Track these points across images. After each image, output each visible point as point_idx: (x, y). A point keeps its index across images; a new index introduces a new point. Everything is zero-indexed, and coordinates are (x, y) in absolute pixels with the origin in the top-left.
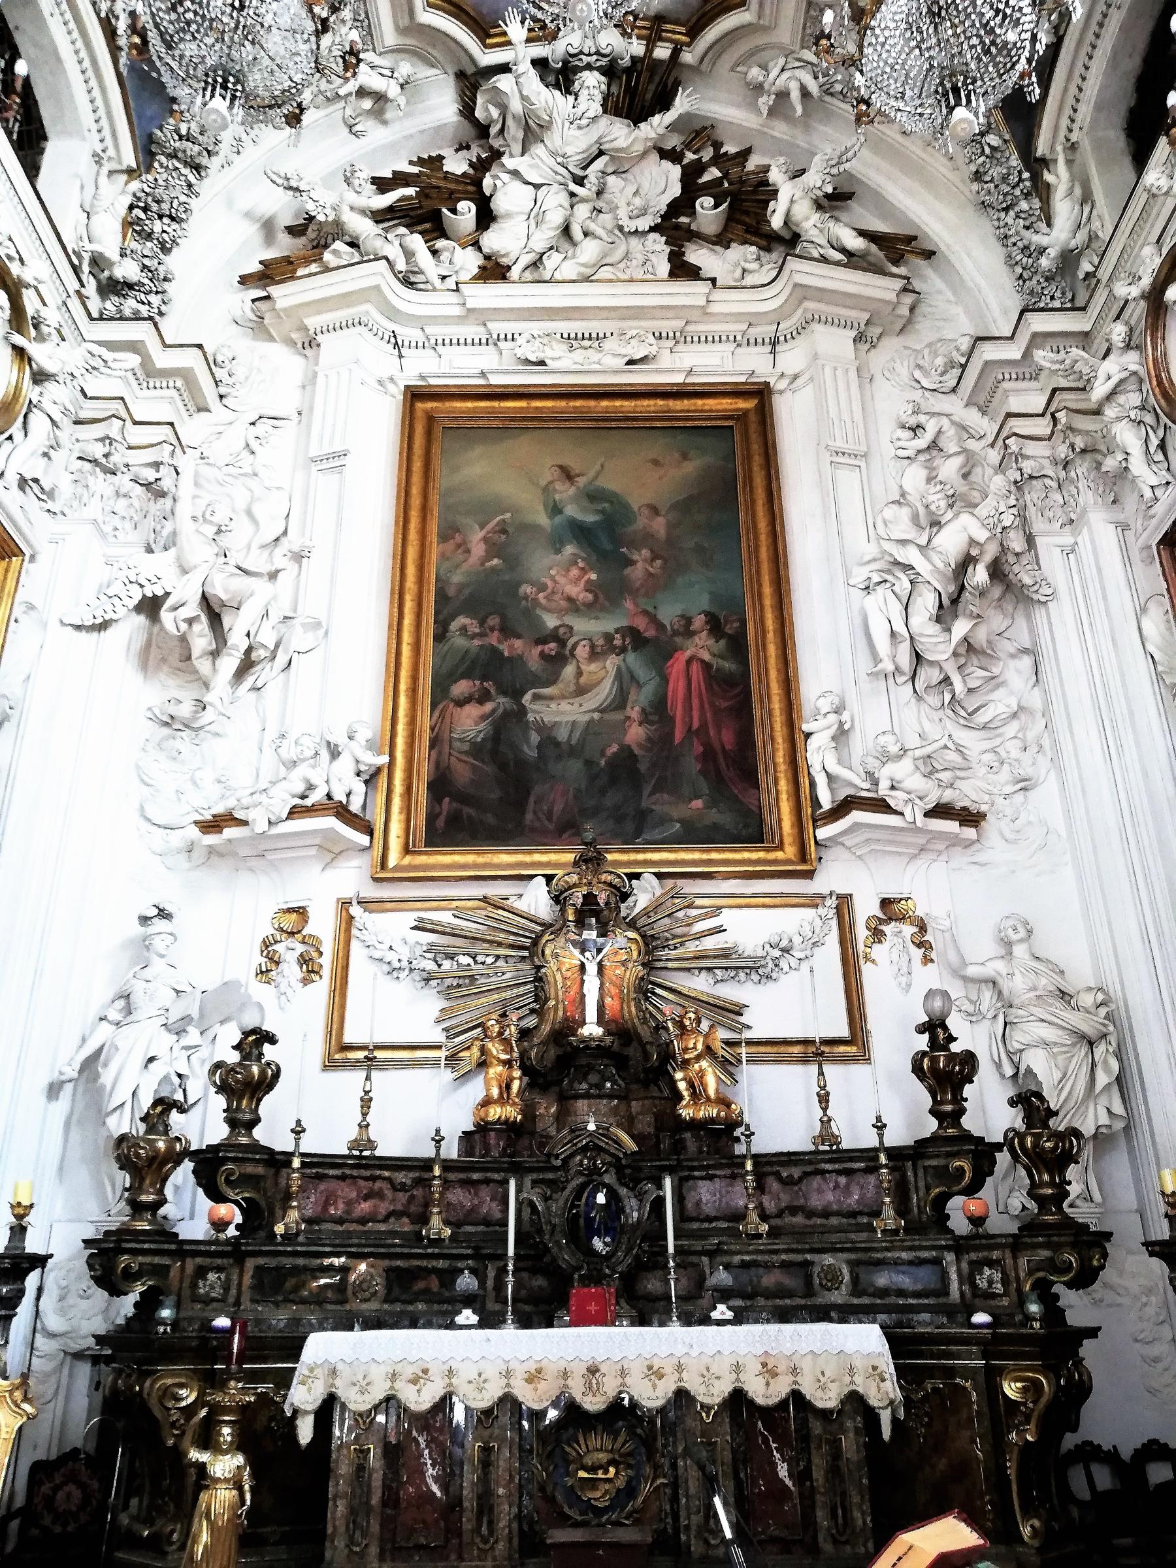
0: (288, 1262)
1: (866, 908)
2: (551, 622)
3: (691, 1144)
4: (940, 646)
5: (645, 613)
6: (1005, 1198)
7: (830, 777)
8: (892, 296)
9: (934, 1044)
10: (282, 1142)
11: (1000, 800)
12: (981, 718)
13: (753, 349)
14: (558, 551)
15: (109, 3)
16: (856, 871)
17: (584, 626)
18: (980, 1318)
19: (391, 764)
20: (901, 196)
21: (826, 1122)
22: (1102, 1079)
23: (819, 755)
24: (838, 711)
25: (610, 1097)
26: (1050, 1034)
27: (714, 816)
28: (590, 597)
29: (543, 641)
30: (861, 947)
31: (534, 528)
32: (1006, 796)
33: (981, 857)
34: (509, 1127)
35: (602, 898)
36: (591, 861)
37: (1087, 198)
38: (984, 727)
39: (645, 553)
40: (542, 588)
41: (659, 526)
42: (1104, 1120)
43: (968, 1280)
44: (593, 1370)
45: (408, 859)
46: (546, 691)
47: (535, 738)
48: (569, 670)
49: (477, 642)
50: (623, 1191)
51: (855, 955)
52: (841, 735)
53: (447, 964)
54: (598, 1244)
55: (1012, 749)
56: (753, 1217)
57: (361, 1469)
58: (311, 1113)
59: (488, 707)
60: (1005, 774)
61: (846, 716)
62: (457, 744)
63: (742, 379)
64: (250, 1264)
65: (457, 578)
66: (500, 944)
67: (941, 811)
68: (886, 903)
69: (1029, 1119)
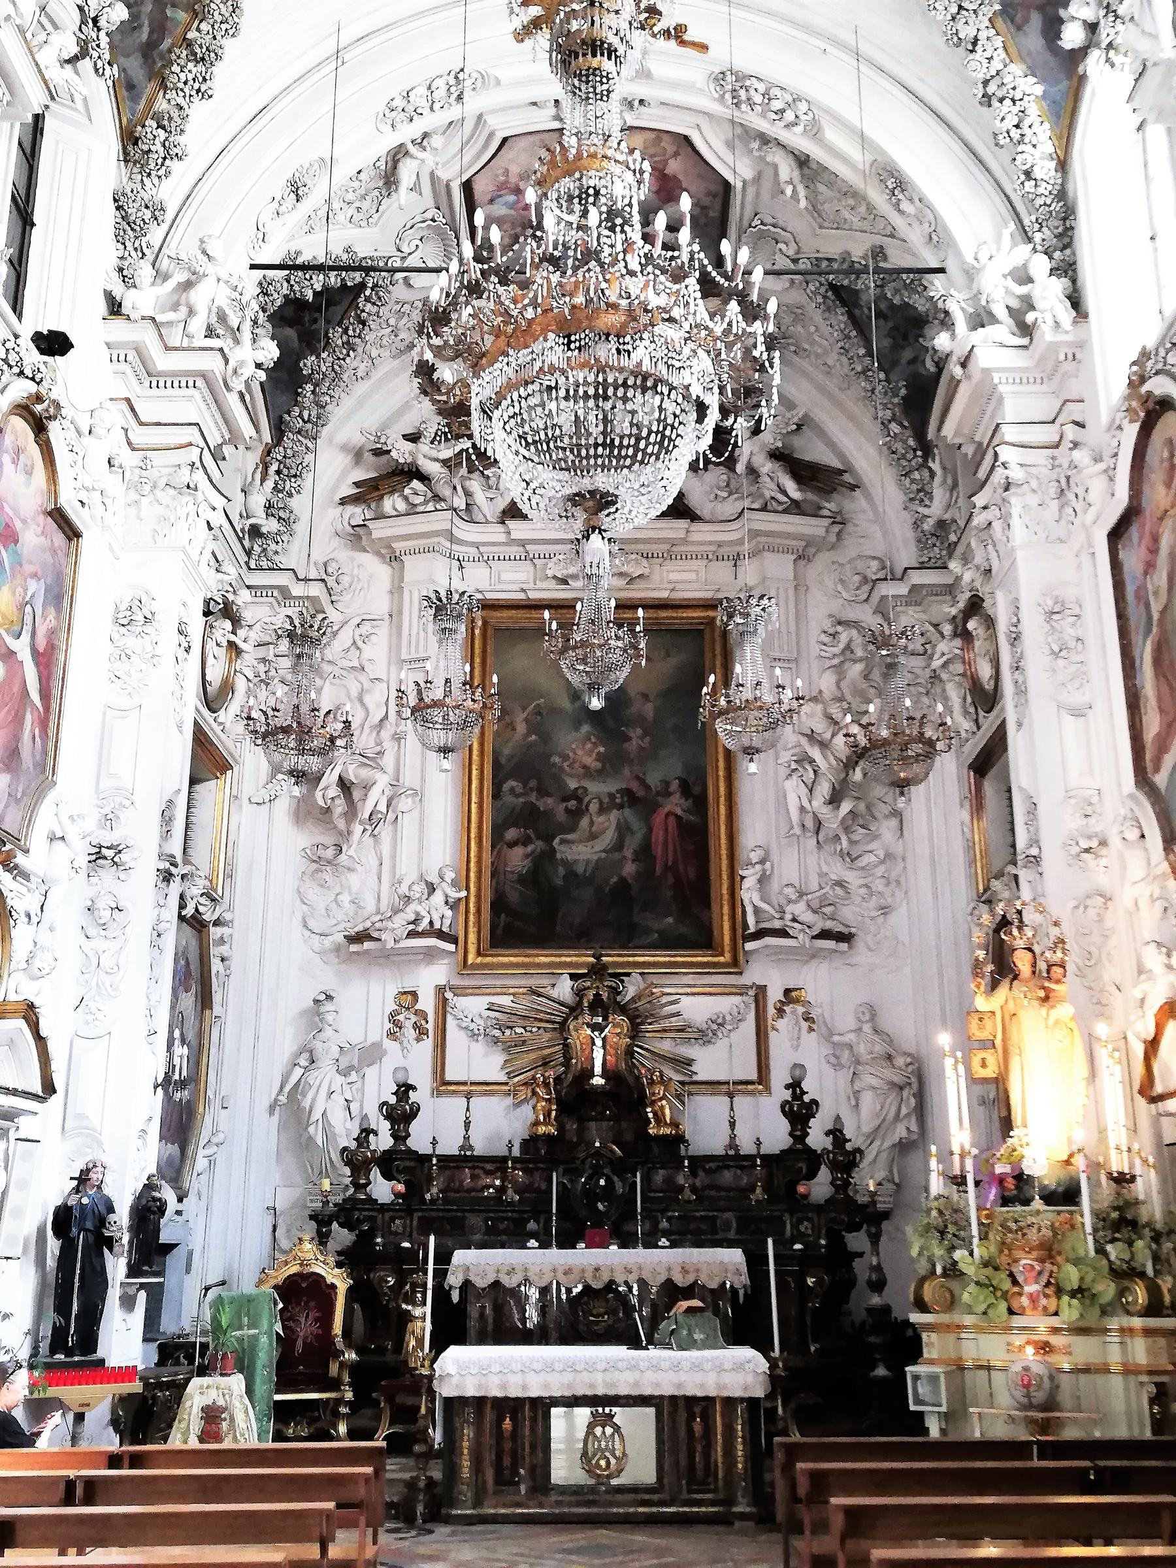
0: (434, 1214)
1: (775, 995)
2: (573, 784)
3: (656, 1150)
4: (833, 820)
5: (638, 778)
6: (820, 1187)
7: (757, 911)
9: (795, 1097)
10: (424, 1148)
11: (868, 920)
12: (862, 862)
13: (721, 563)
14: (577, 729)
16: (768, 972)
17: (597, 788)
18: (798, 1246)
19: (467, 898)
21: (733, 1137)
22: (904, 1111)
23: (749, 893)
24: (762, 862)
25: (609, 1119)
26: (875, 1082)
27: (683, 930)
28: (599, 765)
29: (566, 799)
30: (770, 1021)
31: (559, 711)
32: (872, 918)
33: (852, 961)
34: (548, 1137)
35: (605, 995)
36: (598, 957)
38: (863, 868)
39: (639, 731)
40: (565, 758)
41: (649, 710)
42: (904, 1134)
43: (795, 1227)
44: (597, 1269)
45: (479, 960)
46: (569, 837)
47: (561, 871)
48: (584, 822)
49: (521, 800)
50: (615, 1179)
51: (766, 1027)
52: (763, 880)
53: (508, 1032)
54: (600, 1206)
55: (878, 885)
56: (687, 1192)
57: (482, 1315)
58: (438, 1129)
59: (530, 848)
60: (873, 903)
61: (768, 865)
62: (509, 876)
64: (416, 1215)
65: (506, 751)
66: (541, 1020)
67: (824, 935)
68: (787, 992)
69: (834, 1143)
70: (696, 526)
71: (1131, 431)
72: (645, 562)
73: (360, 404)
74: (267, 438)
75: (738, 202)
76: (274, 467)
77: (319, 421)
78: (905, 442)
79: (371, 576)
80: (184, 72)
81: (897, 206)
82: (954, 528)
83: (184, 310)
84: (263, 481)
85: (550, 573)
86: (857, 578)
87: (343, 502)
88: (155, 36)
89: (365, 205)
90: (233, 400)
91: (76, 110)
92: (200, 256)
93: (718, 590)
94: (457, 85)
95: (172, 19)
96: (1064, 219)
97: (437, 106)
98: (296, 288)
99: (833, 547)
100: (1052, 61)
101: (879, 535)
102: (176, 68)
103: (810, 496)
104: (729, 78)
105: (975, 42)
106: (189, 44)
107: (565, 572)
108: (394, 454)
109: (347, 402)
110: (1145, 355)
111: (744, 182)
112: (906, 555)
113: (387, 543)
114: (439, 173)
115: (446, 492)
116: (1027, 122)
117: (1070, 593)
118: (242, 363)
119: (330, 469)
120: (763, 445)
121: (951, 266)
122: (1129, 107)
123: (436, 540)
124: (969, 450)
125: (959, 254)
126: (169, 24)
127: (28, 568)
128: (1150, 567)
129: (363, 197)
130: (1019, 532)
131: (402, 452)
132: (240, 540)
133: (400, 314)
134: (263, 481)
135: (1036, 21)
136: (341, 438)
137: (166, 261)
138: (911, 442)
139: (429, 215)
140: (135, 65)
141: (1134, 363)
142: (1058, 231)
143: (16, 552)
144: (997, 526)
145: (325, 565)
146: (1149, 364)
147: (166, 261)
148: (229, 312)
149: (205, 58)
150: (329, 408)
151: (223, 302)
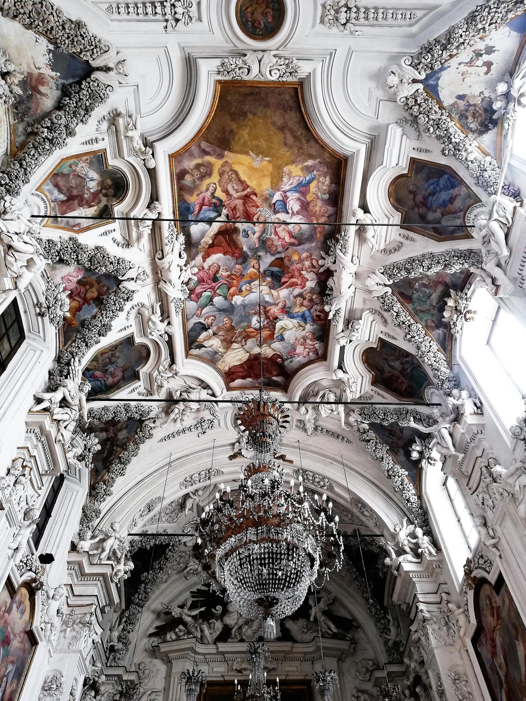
8: (347, 647)
13: (306, 662)
15: (212, 24)
20: (349, 604)
37: (398, 626)
63: (303, 678)
70: (296, 645)
71: (471, 594)
72: (275, 662)
73: (162, 593)
74: (123, 607)
76: (124, 619)
77: (146, 599)
78: (376, 607)
79: (158, 670)
80: (116, 467)
81: (362, 513)
82: (401, 645)
83: (100, 550)
84: (119, 625)
85: (234, 668)
86: (364, 669)
87: (151, 635)
89: (173, 515)
90: (113, 586)
92: (110, 529)
93: (306, 675)
94: (209, 473)
96: (424, 516)
97: (201, 480)
98: (144, 544)
99: (353, 654)
100: (410, 464)
101: (371, 649)
102: (114, 465)
103: (341, 631)
104: (301, 471)
105: (382, 458)
106: (120, 458)
107: (241, 667)
108: (173, 613)
109: (157, 592)
110: (469, 561)
112: (383, 658)
113: (166, 653)
114: (200, 504)
115: (193, 630)
116: (405, 483)
117: (461, 669)
118: (119, 571)
119: (146, 620)
120: (320, 609)
121: (385, 533)
122: (442, 473)
123: (187, 652)
124: (404, 607)
125: (388, 529)
127: (11, 658)
128: (494, 654)
129: (172, 512)
130: (433, 642)
131: (176, 612)
132: (105, 652)
133: (181, 557)
134: (119, 625)
135: (402, 452)
136: (153, 607)
137: (98, 531)
138: (378, 607)
139: (195, 519)
140: (100, 465)
141: (465, 566)
142: (423, 518)
143: (7, 650)
144: (423, 639)
145: (139, 665)
146: (472, 565)
147: (98, 531)
148: (118, 551)
149: (125, 463)
150: (150, 594)
151: (116, 547)
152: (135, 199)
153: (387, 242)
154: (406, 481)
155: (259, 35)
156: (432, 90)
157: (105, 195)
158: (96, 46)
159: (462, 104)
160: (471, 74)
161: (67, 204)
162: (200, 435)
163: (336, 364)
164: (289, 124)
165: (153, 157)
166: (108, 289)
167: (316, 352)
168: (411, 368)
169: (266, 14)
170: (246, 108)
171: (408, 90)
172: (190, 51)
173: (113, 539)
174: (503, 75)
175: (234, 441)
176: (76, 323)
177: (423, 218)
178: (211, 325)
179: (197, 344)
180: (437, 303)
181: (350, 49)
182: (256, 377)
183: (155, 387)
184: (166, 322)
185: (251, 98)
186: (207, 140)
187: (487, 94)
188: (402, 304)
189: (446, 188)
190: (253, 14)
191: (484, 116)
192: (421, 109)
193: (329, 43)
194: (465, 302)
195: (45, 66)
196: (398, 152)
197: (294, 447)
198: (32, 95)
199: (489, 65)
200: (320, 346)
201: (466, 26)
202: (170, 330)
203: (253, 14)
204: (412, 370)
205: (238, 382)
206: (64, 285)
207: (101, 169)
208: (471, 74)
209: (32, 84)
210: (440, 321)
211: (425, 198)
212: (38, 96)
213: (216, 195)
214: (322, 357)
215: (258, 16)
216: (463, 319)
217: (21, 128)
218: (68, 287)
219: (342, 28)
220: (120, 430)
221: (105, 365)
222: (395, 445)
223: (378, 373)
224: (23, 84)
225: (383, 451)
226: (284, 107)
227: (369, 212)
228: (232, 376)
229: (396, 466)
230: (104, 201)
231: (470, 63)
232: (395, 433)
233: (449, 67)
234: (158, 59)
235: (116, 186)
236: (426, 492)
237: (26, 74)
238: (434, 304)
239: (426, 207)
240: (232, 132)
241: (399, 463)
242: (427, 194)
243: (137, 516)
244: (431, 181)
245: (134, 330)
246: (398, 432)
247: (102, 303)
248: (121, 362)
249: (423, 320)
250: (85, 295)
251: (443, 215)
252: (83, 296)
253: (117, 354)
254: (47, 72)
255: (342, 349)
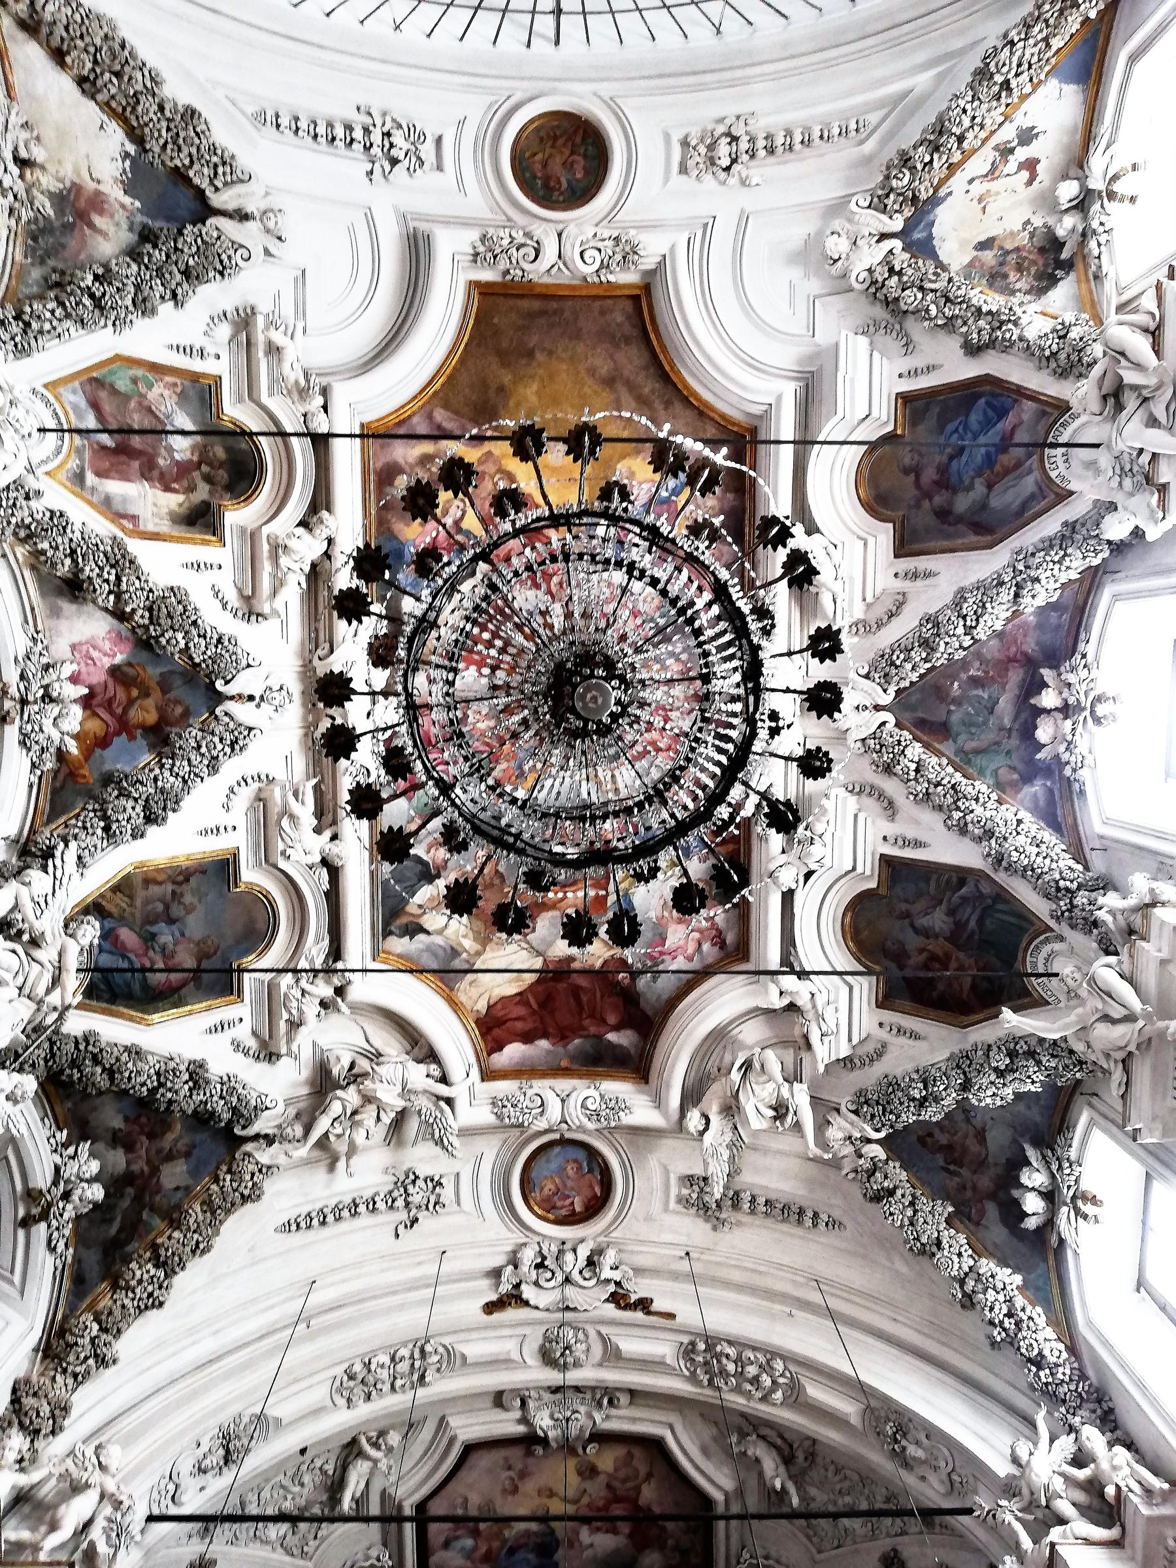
75: (722, 1549)
88: (123, 1236)
91: (11, 1282)
95: (146, 1224)
100: (1022, 1248)
102: (134, 1265)
105: (939, 1244)
106: (155, 1247)
111: (726, 1494)
126: (141, 1229)
135: (992, 1211)
139: (374, 1553)
140: (92, 1258)
149: (169, 1267)
152: (297, 931)
153: (869, 599)
154: (1020, 1301)
155: (557, 202)
156: (920, 245)
157: (208, 479)
158: (223, 165)
159: (989, 256)
160: (998, 193)
161: (114, 459)
162: (401, 1229)
163: (773, 959)
164: (626, 373)
165: (326, 411)
166: (186, 714)
167: (719, 939)
168: (978, 912)
169: (572, 164)
170: (534, 340)
171: (871, 256)
172: (417, 224)
173: (92, 1496)
174: (1068, 167)
175: (499, 1261)
176: (89, 774)
177: (943, 514)
178: (445, 867)
179: (404, 920)
180: (1016, 718)
181: (742, 211)
182: (562, 1036)
183: (283, 1027)
184: (327, 834)
185: (542, 321)
186: (446, 406)
187: (1038, 222)
188: (926, 746)
189: (987, 424)
190: (545, 165)
191: (1041, 262)
192: (905, 278)
193: (703, 209)
194: (1084, 674)
195: (111, 181)
196: (869, 389)
197: (675, 1276)
198: (74, 224)
199: (1030, 165)
200: (727, 921)
201: (970, 93)
202: (335, 849)
203: (545, 165)
204: (980, 921)
205: (513, 1052)
206: (75, 667)
207: (203, 417)
208: (998, 193)
209: (77, 205)
210: (1030, 761)
211: (943, 470)
212: (87, 231)
213: (465, 525)
214: (733, 953)
215: (556, 167)
216: (1089, 720)
217: (36, 274)
218: (84, 676)
219: (723, 175)
220: (170, 1157)
221: (151, 919)
222: (969, 1194)
223: (893, 966)
224: (60, 199)
225: (935, 1216)
226: (614, 337)
227: (818, 531)
228: (496, 1032)
229: (984, 1261)
230: (202, 492)
231: (992, 173)
232: (965, 1150)
233: (950, 193)
234: (352, 231)
235: (234, 464)
236: (1089, 1323)
237: (68, 184)
238: (1007, 722)
239: (947, 488)
240: (501, 389)
241: (991, 1255)
242: (945, 459)
243: (186, 1466)
244: (950, 427)
245: (239, 840)
246: (973, 1146)
247: (166, 741)
248: (195, 926)
249: (988, 773)
250: (125, 711)
251: (990, 487)
252: (119, 711)
253: (188, 899)
254: (115, 193)
255: (788, 897)
